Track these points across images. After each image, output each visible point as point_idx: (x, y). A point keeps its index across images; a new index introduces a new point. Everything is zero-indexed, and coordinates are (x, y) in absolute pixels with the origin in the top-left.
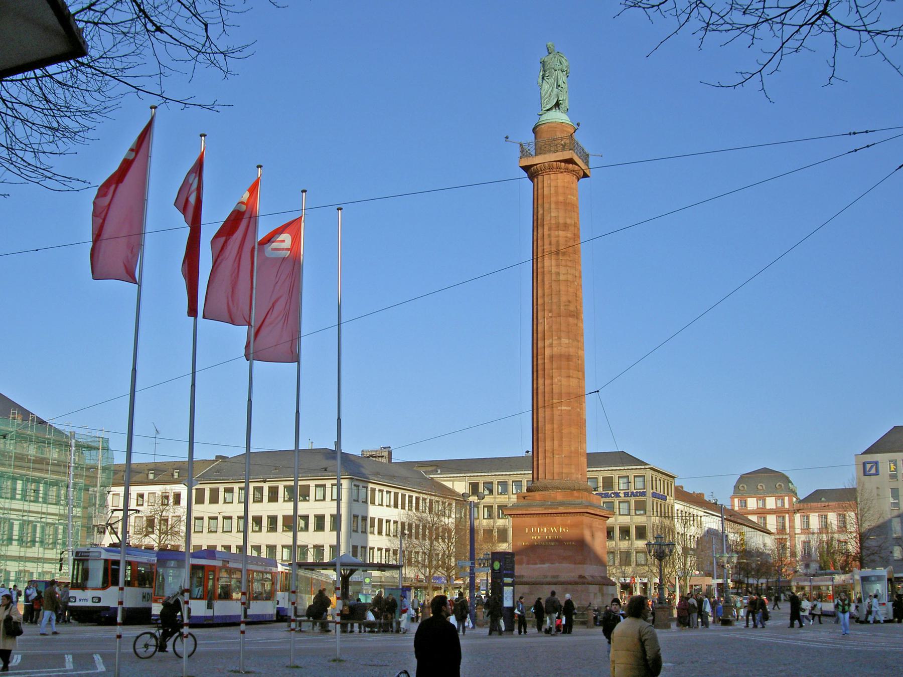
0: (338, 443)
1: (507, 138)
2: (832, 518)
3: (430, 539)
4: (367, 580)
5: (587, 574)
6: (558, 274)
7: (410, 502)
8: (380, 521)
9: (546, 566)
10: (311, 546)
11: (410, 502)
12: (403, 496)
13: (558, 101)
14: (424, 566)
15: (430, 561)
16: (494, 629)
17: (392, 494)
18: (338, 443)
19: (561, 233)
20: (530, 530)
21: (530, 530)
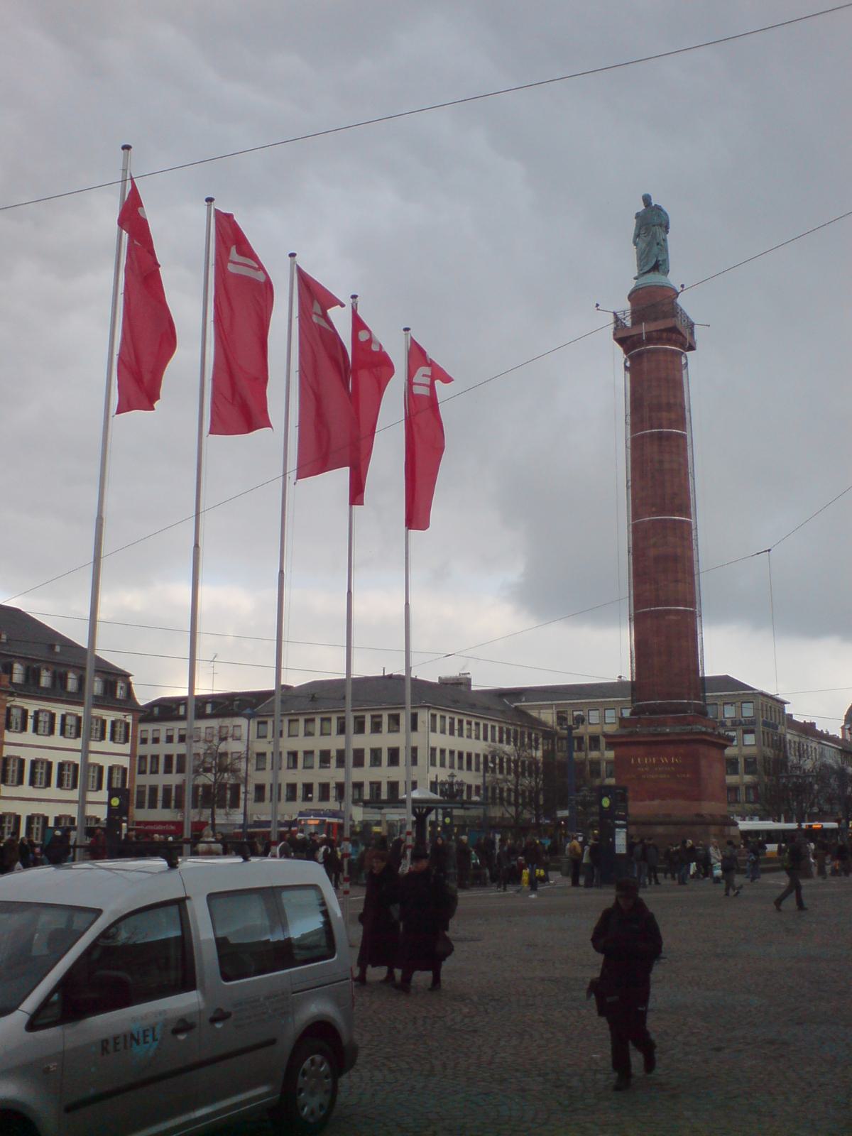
0: (408, 669)
1: (597, 305)
2: (398, 973)
3: (516, 773)
4: (808, 811)
5: (704, 812)
6: (661, 462)
7: (452, 725)
8: (443, 751)
9: (656, 802)
10: (332, 785)
11: (452, 725)
12: (485, 727)
13: (657, 262)
14: (510, 804)
15: (516, 799)
16: (575, 883)
17: (481, 726)
18: (408, 669)
19: (665, 414)
20: (636, 760)
21: (636, 760)
